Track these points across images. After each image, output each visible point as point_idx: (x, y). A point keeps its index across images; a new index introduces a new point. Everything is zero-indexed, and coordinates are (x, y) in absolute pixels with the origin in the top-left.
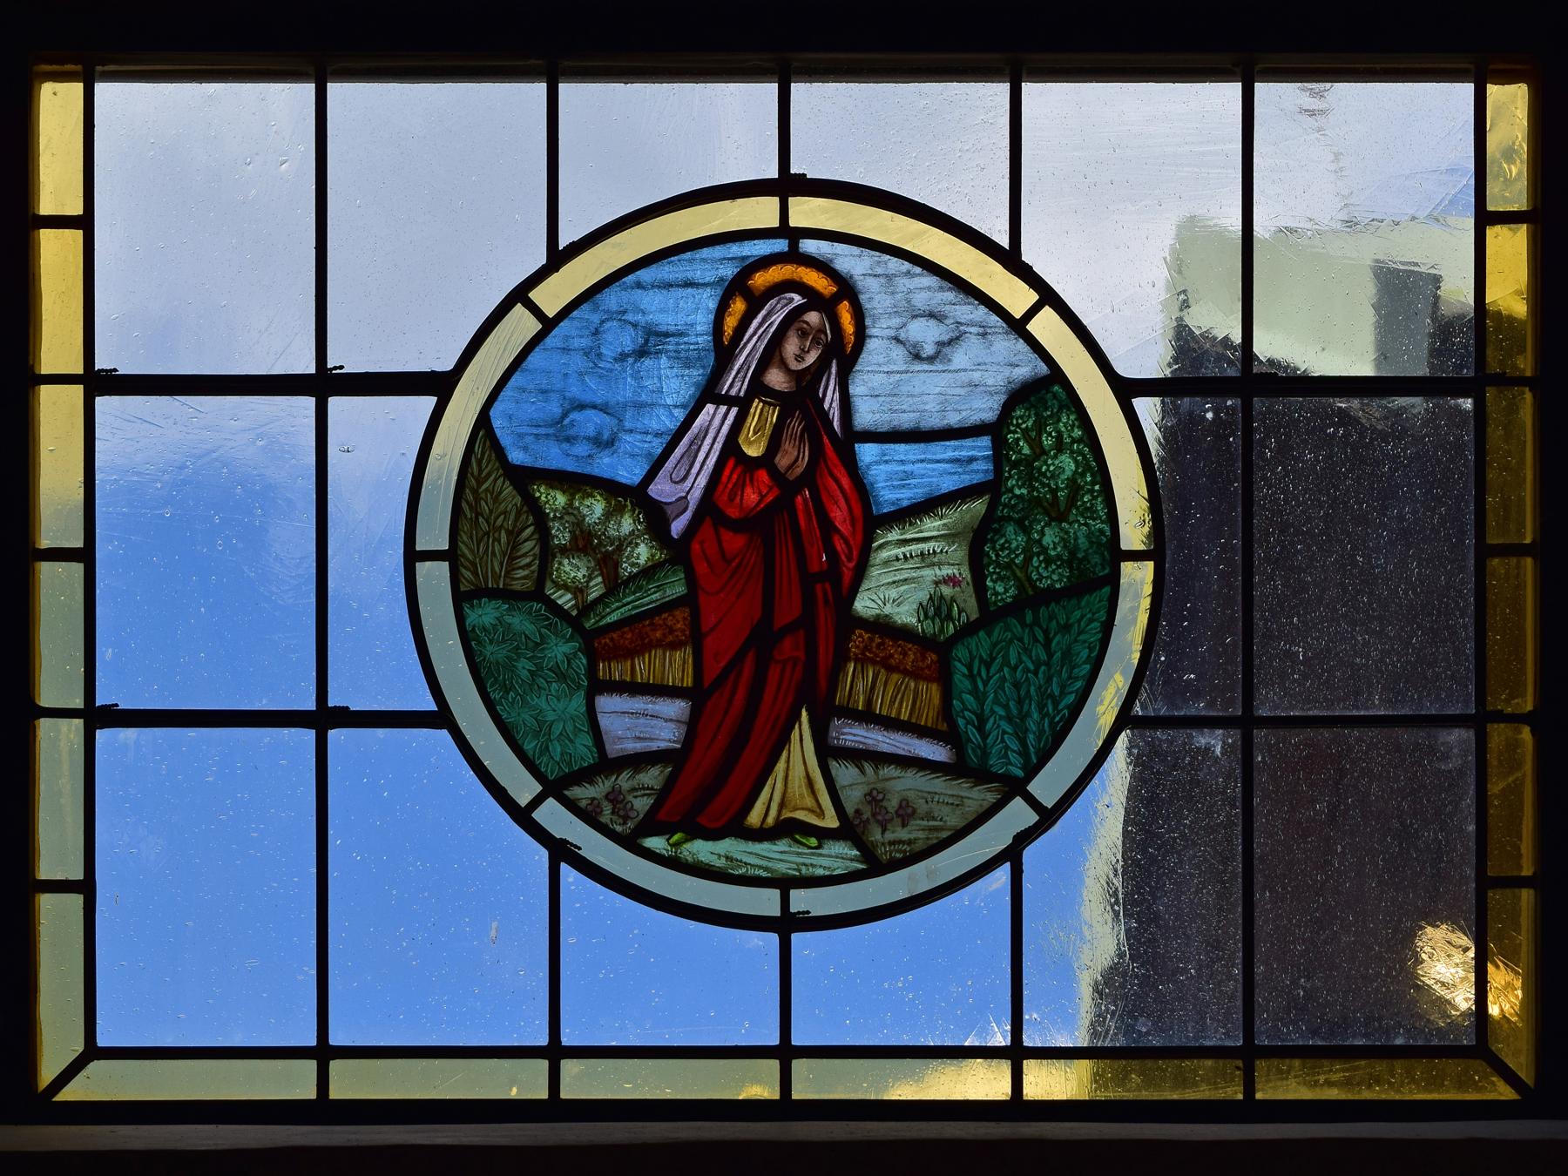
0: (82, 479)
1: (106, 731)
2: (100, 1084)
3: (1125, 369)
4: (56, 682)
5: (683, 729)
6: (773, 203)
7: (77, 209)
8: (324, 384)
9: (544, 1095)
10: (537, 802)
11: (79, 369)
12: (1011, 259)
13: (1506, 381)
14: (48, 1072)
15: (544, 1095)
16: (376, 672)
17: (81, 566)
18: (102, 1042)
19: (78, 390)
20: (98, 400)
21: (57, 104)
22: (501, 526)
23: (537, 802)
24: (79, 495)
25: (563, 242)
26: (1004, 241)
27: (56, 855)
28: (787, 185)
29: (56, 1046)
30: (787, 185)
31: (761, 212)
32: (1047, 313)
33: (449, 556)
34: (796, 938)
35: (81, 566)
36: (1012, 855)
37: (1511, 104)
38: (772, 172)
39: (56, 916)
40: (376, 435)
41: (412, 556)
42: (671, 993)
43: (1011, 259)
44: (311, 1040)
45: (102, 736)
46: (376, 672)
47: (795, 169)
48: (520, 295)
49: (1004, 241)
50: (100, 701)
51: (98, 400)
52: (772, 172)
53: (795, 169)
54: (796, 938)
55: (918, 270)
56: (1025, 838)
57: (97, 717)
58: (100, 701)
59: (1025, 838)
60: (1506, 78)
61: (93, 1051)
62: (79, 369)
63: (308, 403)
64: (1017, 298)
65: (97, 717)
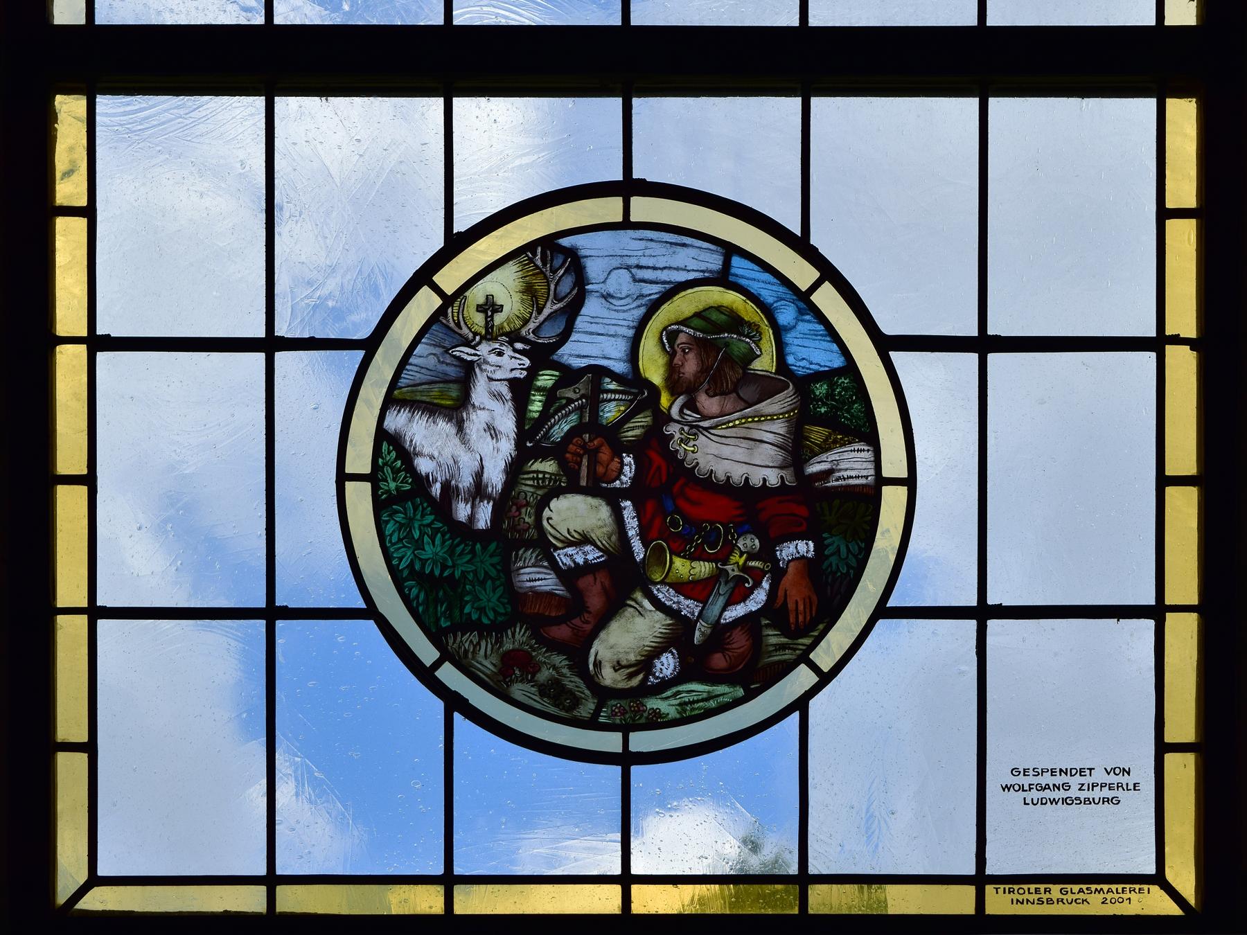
2: (99, 900)
6: (618, 202)
10: (437, 664)
11: (84, 333)
12: (801, 245)
13: (1177, 340)
17: (85, 488)
18: (102, 871)
21: (69, 107)
23: (437, 664)
26: (797, 230)
28: (629, 187)
30: (629, 187)
32: (827, 287)
33: (373, 478)
34: (634, 769)
35: (85, 488)
36: (801, 705)
37: (1184, 114)
38: (618, 176)
40: (311, 386)
41: (342, 478)
44: (262, 870)
45: (101, 357)
47: (636, 175)
48: (825, 678)
49: (797, 230)
50: (100, 331)
53: (636, 175)
54: (634, 769)
55: (756, 268)
57: (96, 343)
58: (100, 331)
61: (94, 880)
62: (84, 333)
63: (259, 358)
65: (96, 343)
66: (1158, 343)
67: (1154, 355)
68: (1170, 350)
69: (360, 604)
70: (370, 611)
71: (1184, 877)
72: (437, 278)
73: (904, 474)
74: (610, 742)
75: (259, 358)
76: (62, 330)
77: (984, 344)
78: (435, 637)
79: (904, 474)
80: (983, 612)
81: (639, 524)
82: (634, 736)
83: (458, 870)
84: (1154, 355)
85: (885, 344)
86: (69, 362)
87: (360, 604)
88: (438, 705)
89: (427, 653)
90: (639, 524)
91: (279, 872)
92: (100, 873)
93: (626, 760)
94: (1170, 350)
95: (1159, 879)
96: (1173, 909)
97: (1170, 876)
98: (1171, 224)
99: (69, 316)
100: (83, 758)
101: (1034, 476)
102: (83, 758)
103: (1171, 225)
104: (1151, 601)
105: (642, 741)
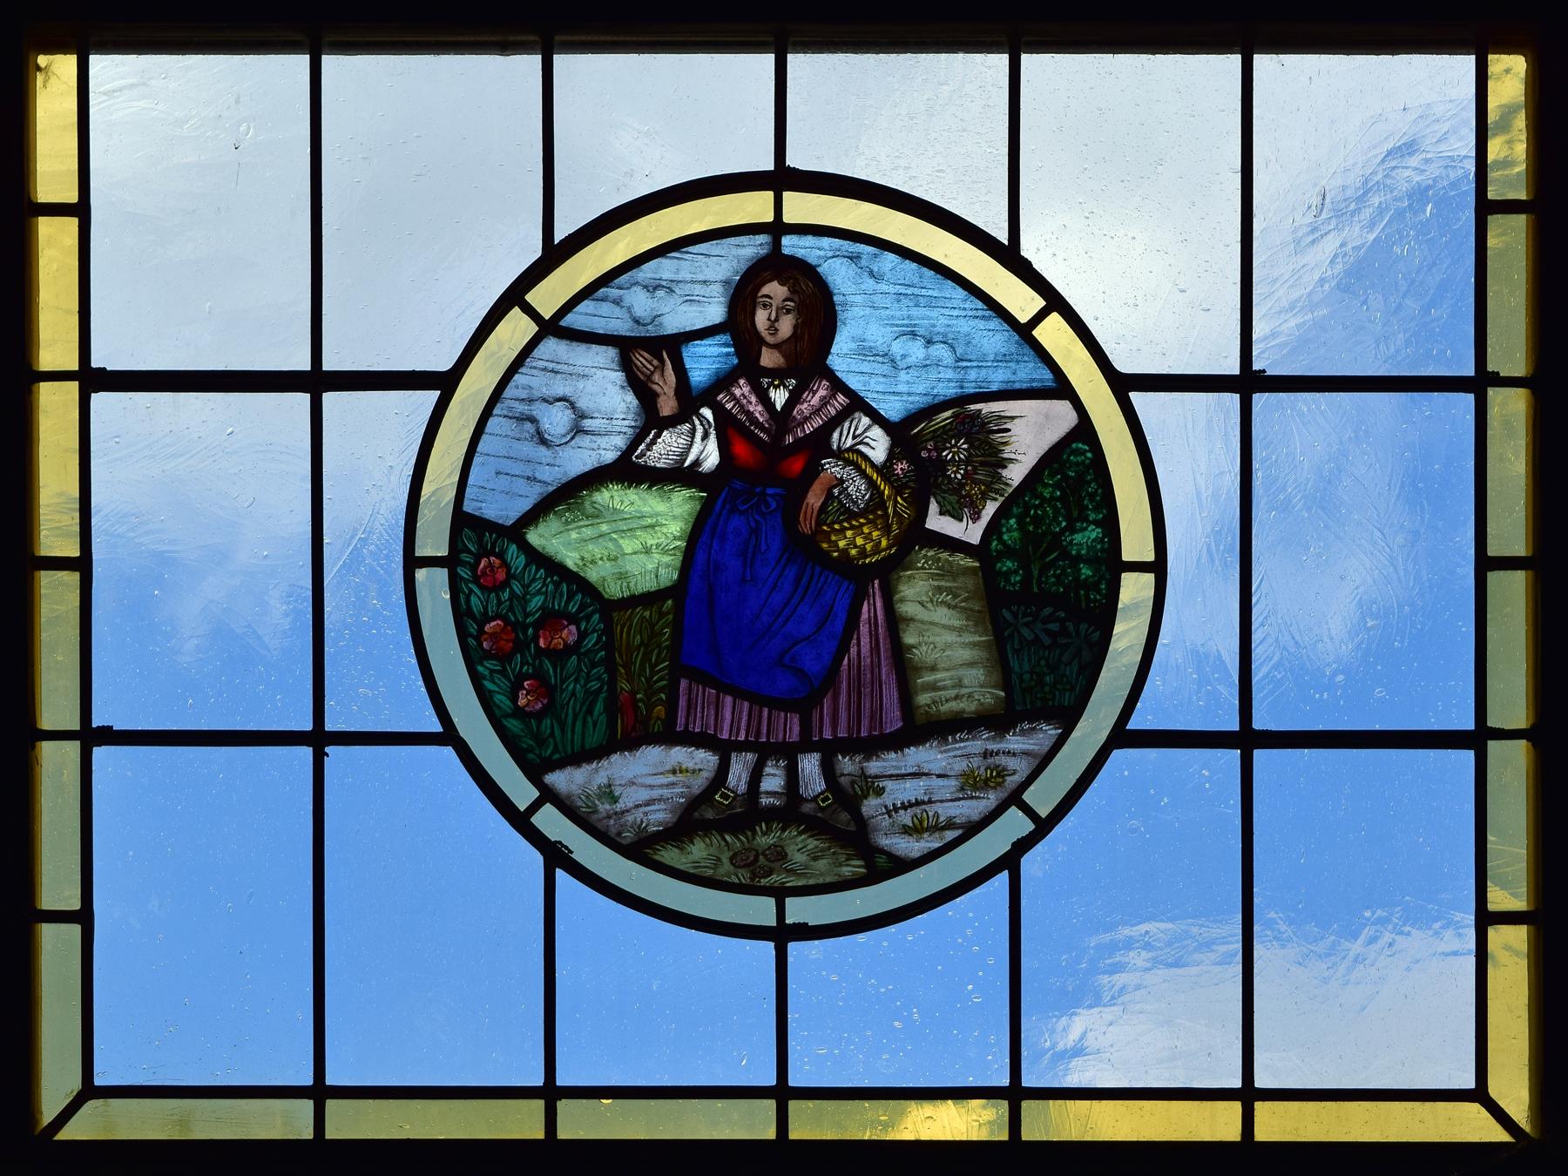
0: (77, 604)
1: (104, 748)
3: (1124, 365)
4: (56, 706)
5: (680, 556)
7: (72, 197)
8: (316, 382)
9: (540, 1135)
10: (535, 807)
11: (75, 725)
12: (1009, 255)
14: (49, 1111)
15: (540, 1135)
16: (374, 688)
17: (76, 220)
19: (74, 386)
20: (96, 750)
21: (55, 78)
22: (498, 590)
23: (535, 807)
24: (75, 492)
25: (559, 235)
26: (1003, 236)
27: (56, 886)
28: (782, 179)
29: (56, 1083)
30: (782, 179)
31: (756, 206)
35: (76, 220)
36: (1010, 862)
37: (1511, 74)
38: (768, 164)
39: (56, 947)
41: (412, 562)
42: (672, 1008)
43: (1009, 255)
45: (98, 400)
46: (374, 688)
48: (1043, 827)
49: (1003, 236)
50: (97, 722)
51: (96, 750)
52: (768, 164)
56: (1023, 845)
57: (92, 380)
58: (97, 722)
59: (1023, 845)
60: (1507, 46)
61: (89, 1091)
62: (75, 725)
63: (303, 400)
64: (1022, 301)
65: (92, 380)
66: (1477, 739)
67: (1471, 753)
68: (1493, 746)
69: (436, 727)
70: (449, 736)
71: (1514, 1089)
72: (529, 298)
73: (1150, 556)
74: (760, 911)
75: (303, 400)
76: (47, 722)
77: (1248, 383)
78: (534, 773)
79: (1150, 556)
80: (1247, 739)
81: (798, 616)
82: (791, 903)
83: (562, 1080)
84: (1471, 753)
85: (1122, 385)
86: (55, 406)
87: (436, 727)
88: (537, 859)
89: (522, 792)
90: (798, 616)
91: (328, 727)
92: (98, 1082)
93: (783, 935)
94: (1493, 746)
95: (1479, 1094)
96: (1500, 1135)
97: (1494, 1091)
98: (1494, 578)
99: (55, 347)
100: (73, 578)
101: (1321, 563)
102: (73, 578)
103: (1495, 222)
104: (1470, 725)
105: (800, 910)
